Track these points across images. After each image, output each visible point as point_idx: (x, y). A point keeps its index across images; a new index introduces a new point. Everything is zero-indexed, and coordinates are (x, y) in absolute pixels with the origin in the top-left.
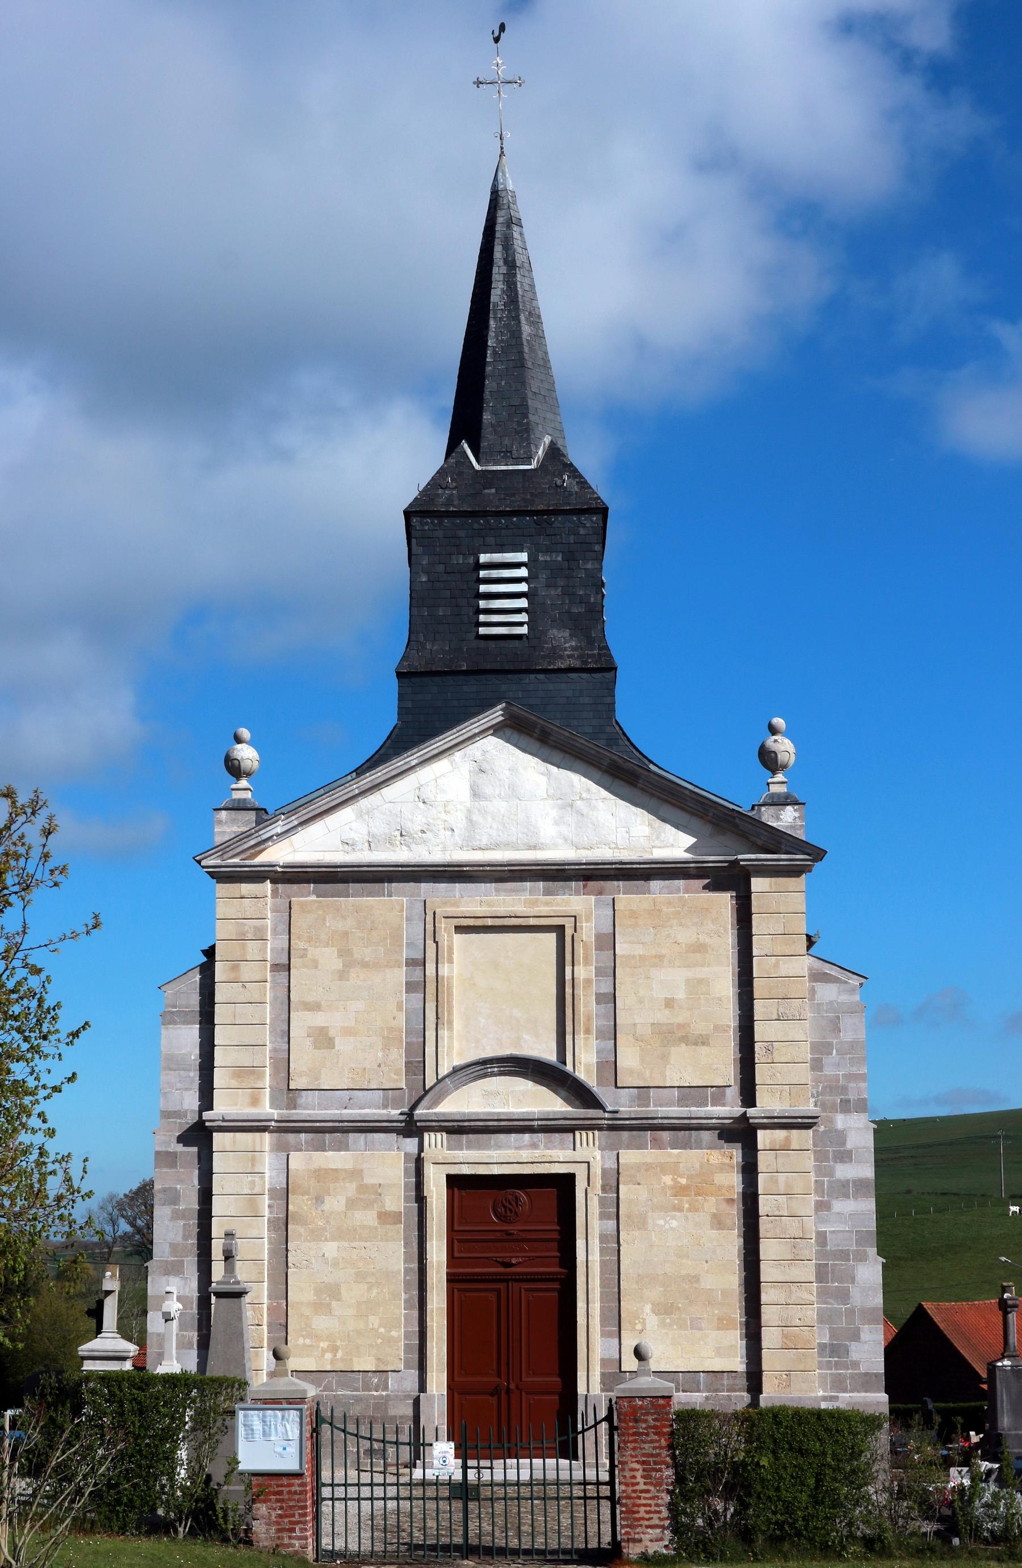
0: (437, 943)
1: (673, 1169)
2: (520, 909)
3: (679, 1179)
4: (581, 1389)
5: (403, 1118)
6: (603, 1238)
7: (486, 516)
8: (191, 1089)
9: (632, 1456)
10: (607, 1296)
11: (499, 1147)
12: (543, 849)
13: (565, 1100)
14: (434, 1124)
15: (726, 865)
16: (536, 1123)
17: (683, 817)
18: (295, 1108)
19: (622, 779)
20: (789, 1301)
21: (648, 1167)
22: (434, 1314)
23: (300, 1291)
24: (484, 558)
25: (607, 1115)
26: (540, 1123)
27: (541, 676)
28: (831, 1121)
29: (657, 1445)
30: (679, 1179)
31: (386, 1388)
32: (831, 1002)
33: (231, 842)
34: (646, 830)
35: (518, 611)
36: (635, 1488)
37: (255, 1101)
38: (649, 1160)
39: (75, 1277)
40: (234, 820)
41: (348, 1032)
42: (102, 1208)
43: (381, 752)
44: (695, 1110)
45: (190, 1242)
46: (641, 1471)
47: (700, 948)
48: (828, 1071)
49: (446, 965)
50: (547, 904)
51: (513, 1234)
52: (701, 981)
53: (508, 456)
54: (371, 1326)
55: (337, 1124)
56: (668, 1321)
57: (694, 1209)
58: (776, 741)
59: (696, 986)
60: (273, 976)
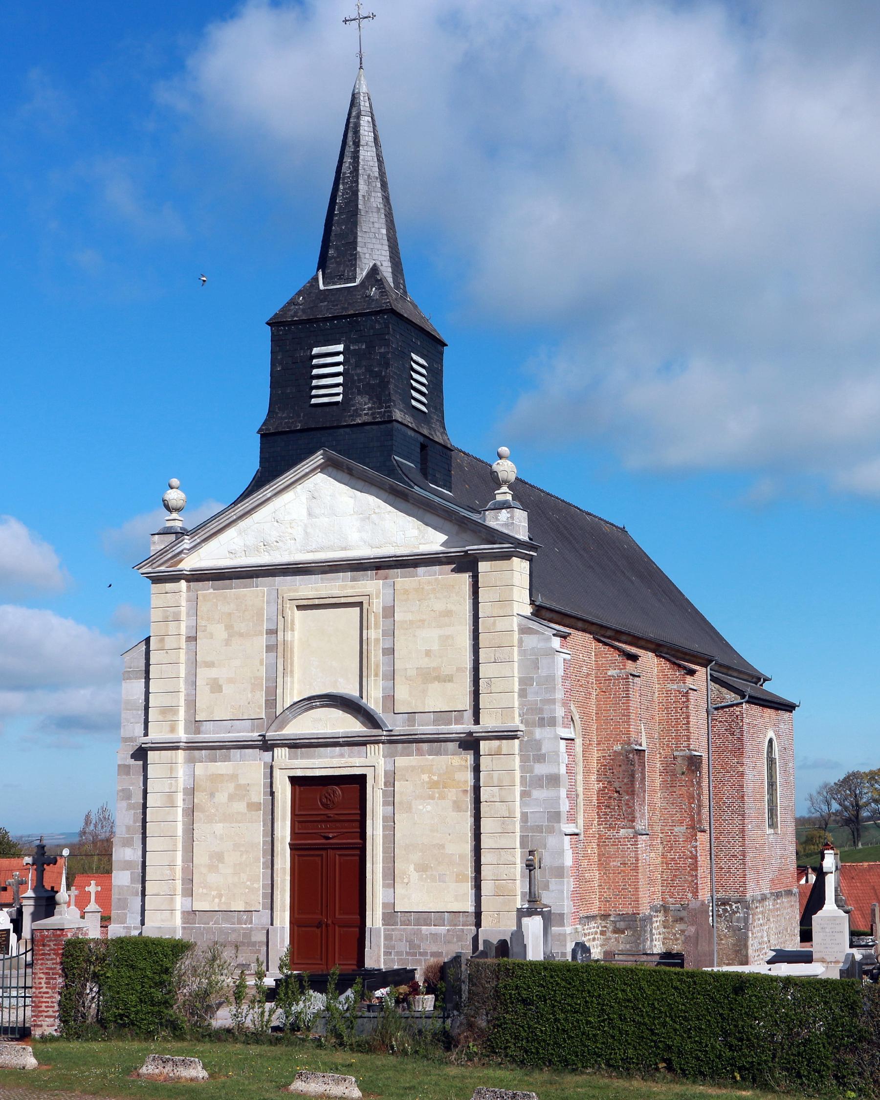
0: (283, 617)
1: (423, 770)
2: (336, 592)
3: (433, 777)
4: (369, 924)
5: (260, 738)
6: (385, 819)
7: (317, 322)
8: (139, 723)
9: (40, 969)
10: (387, 859)
11: (320, 757)
12: (351, 549)
13: (362, 723)
14: (279, 742)
15: (462, 554)
16: (341, 740)
17: (440, 521)
18: (199, 734)
19: (401, 498)
20: (499, 862)
21: (413, 768)
22: (279, 872)
23: (200, 857)
24: (315, 351)
25: (385, 733)
26: (344, 739)
27: (348, 430)
28: (531, 733)
29: (54, 961)
30: (433, 777)
31: (251, 923)
32: (533, 648)
33: (155, 556)
34: (416, 532)
35: (337, 385)
36: (41, 990)
37: (173, 729)
38: (414, 763)
39: (818, 842)
40: (163, 541)
41: (231, 681)
42: (819, 793)
43: (249, 489)
44: (443, 728)
45: (138, 824)
46: (44, 979)
47: (448, 613)
48: (531, 698)
49: (290, 632)
50: (352, 587)
51: (331, 817)
52: (448, 637)
53: (341, 278)
54: (242, 880)
55: (222, 744)
56: (424, 876)
57: (442, 797)
58: (498, 464)
59: (445, 640)
60: (187, 645)
